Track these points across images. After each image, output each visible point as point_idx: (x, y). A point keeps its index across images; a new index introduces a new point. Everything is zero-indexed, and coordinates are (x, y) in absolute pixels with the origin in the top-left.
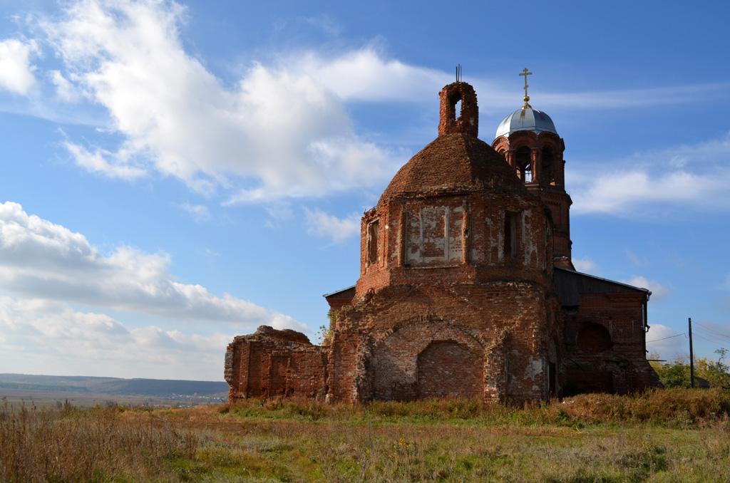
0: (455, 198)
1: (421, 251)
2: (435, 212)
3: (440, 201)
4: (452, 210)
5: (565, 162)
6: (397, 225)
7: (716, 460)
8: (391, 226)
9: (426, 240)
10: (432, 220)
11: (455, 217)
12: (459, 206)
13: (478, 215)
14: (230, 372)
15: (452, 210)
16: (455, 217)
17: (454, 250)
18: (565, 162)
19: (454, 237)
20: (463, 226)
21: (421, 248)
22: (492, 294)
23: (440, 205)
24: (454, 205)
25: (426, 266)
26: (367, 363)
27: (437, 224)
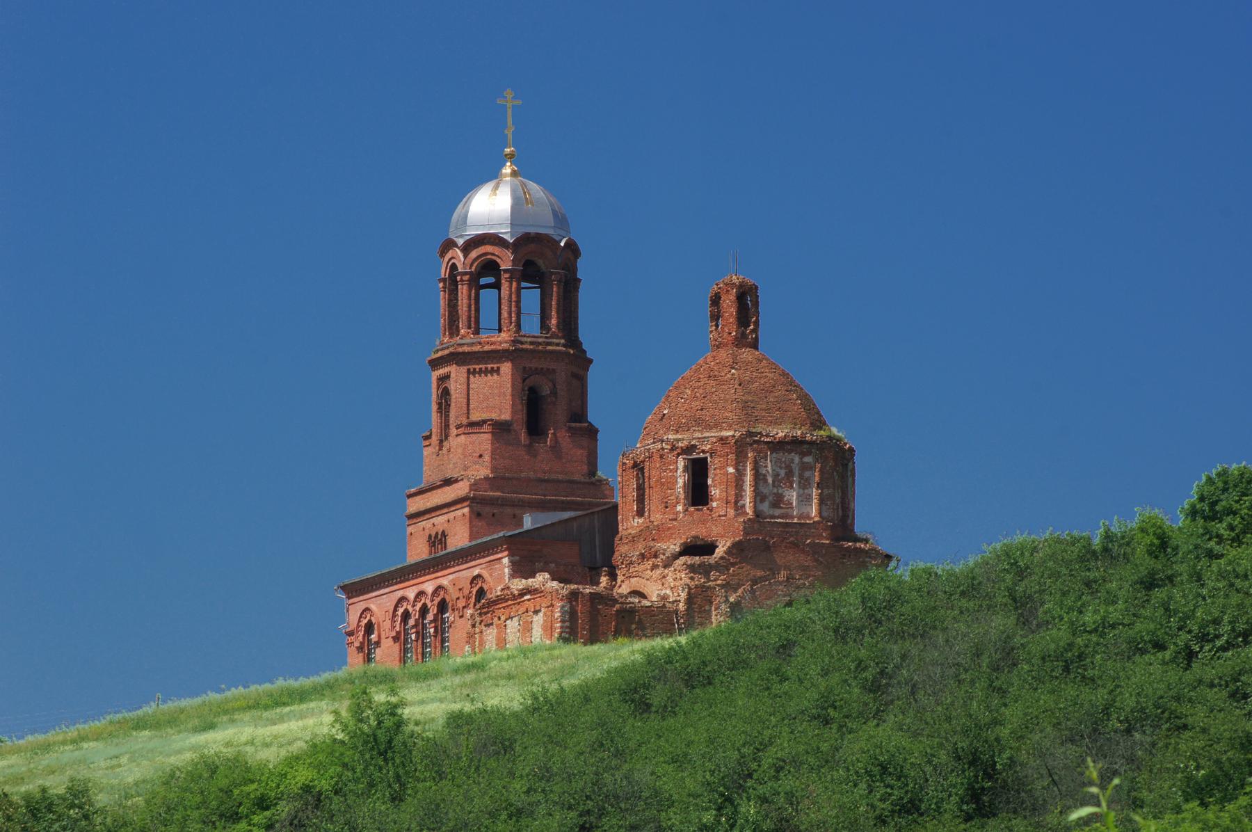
0: (805, 446)
1: (770, 502)
2: (783, 459)
3: (789, 447)
4: (801, 459)
5: (580, 280)
6: (745, 470)
7: (997, 678)
8: (737, 469)
9: (775, 491)
10: (781, 468)
11: (805, 467)
12: (808, 456)
13: (828, 468)
14: (567, 627)
15: (801, 459)
16: (805, 467)
17: (804, 503)
18: (580, 280)
19: (804, 489)
20: (817, 479)
21: (771, 498)
22: (844, 555)
23: (790, 452)
24: (803, 454)
25: (775, 518)
26: (479, 602)
27: (786, 474)
